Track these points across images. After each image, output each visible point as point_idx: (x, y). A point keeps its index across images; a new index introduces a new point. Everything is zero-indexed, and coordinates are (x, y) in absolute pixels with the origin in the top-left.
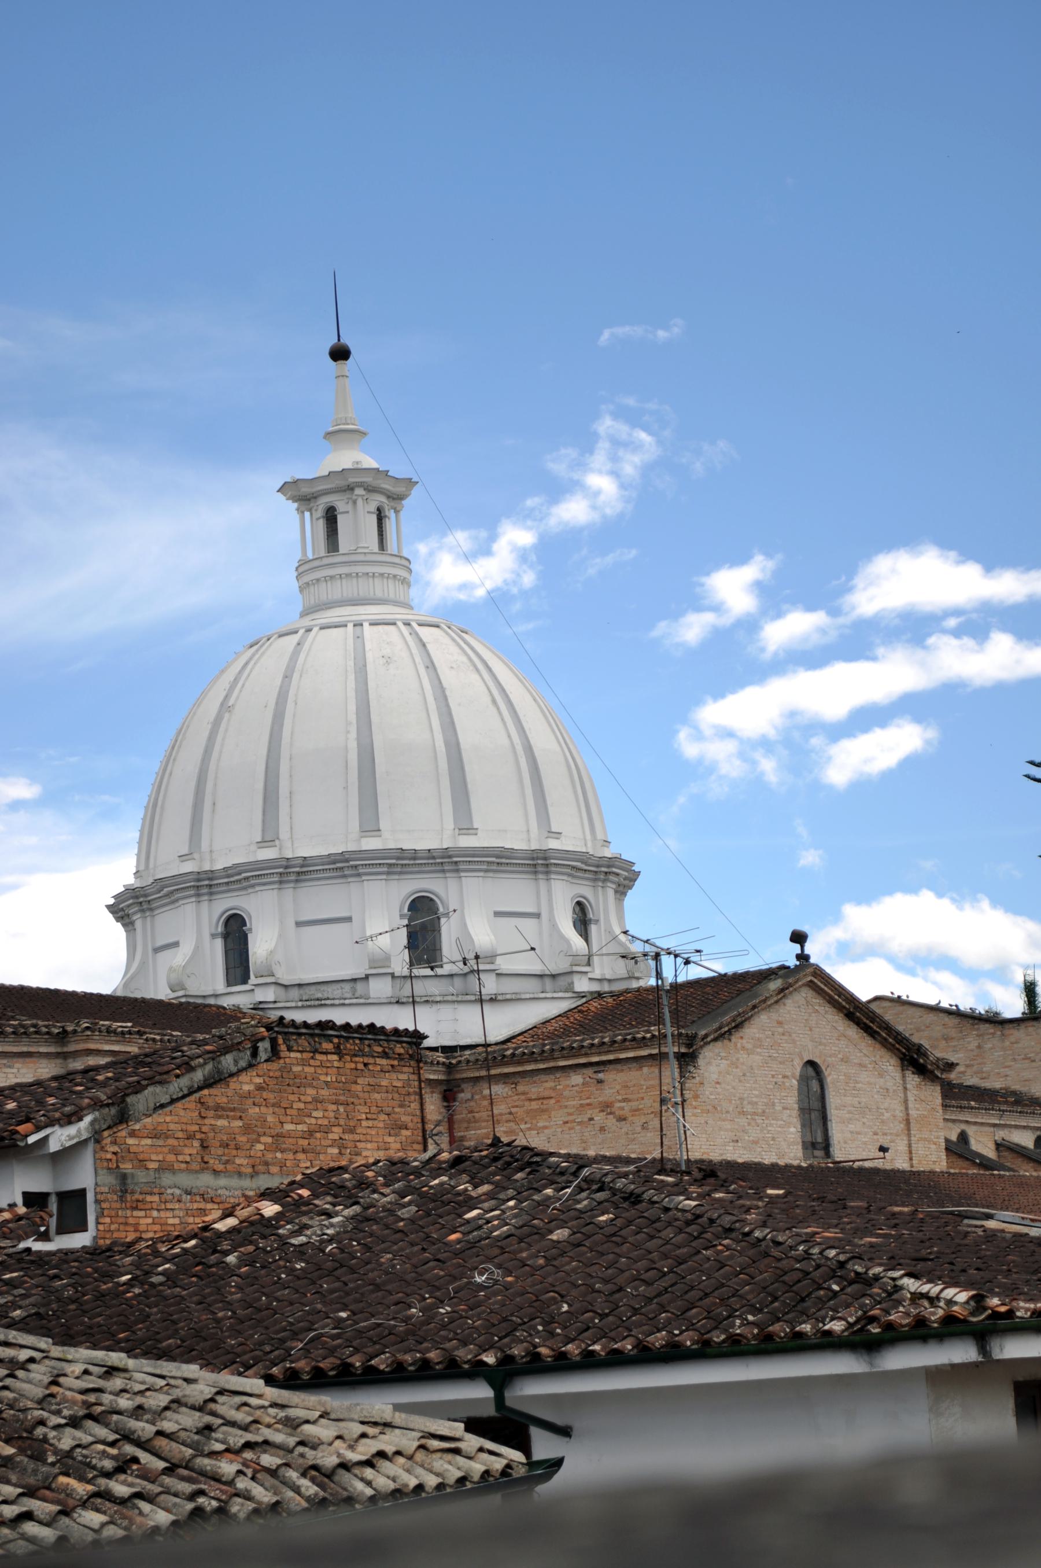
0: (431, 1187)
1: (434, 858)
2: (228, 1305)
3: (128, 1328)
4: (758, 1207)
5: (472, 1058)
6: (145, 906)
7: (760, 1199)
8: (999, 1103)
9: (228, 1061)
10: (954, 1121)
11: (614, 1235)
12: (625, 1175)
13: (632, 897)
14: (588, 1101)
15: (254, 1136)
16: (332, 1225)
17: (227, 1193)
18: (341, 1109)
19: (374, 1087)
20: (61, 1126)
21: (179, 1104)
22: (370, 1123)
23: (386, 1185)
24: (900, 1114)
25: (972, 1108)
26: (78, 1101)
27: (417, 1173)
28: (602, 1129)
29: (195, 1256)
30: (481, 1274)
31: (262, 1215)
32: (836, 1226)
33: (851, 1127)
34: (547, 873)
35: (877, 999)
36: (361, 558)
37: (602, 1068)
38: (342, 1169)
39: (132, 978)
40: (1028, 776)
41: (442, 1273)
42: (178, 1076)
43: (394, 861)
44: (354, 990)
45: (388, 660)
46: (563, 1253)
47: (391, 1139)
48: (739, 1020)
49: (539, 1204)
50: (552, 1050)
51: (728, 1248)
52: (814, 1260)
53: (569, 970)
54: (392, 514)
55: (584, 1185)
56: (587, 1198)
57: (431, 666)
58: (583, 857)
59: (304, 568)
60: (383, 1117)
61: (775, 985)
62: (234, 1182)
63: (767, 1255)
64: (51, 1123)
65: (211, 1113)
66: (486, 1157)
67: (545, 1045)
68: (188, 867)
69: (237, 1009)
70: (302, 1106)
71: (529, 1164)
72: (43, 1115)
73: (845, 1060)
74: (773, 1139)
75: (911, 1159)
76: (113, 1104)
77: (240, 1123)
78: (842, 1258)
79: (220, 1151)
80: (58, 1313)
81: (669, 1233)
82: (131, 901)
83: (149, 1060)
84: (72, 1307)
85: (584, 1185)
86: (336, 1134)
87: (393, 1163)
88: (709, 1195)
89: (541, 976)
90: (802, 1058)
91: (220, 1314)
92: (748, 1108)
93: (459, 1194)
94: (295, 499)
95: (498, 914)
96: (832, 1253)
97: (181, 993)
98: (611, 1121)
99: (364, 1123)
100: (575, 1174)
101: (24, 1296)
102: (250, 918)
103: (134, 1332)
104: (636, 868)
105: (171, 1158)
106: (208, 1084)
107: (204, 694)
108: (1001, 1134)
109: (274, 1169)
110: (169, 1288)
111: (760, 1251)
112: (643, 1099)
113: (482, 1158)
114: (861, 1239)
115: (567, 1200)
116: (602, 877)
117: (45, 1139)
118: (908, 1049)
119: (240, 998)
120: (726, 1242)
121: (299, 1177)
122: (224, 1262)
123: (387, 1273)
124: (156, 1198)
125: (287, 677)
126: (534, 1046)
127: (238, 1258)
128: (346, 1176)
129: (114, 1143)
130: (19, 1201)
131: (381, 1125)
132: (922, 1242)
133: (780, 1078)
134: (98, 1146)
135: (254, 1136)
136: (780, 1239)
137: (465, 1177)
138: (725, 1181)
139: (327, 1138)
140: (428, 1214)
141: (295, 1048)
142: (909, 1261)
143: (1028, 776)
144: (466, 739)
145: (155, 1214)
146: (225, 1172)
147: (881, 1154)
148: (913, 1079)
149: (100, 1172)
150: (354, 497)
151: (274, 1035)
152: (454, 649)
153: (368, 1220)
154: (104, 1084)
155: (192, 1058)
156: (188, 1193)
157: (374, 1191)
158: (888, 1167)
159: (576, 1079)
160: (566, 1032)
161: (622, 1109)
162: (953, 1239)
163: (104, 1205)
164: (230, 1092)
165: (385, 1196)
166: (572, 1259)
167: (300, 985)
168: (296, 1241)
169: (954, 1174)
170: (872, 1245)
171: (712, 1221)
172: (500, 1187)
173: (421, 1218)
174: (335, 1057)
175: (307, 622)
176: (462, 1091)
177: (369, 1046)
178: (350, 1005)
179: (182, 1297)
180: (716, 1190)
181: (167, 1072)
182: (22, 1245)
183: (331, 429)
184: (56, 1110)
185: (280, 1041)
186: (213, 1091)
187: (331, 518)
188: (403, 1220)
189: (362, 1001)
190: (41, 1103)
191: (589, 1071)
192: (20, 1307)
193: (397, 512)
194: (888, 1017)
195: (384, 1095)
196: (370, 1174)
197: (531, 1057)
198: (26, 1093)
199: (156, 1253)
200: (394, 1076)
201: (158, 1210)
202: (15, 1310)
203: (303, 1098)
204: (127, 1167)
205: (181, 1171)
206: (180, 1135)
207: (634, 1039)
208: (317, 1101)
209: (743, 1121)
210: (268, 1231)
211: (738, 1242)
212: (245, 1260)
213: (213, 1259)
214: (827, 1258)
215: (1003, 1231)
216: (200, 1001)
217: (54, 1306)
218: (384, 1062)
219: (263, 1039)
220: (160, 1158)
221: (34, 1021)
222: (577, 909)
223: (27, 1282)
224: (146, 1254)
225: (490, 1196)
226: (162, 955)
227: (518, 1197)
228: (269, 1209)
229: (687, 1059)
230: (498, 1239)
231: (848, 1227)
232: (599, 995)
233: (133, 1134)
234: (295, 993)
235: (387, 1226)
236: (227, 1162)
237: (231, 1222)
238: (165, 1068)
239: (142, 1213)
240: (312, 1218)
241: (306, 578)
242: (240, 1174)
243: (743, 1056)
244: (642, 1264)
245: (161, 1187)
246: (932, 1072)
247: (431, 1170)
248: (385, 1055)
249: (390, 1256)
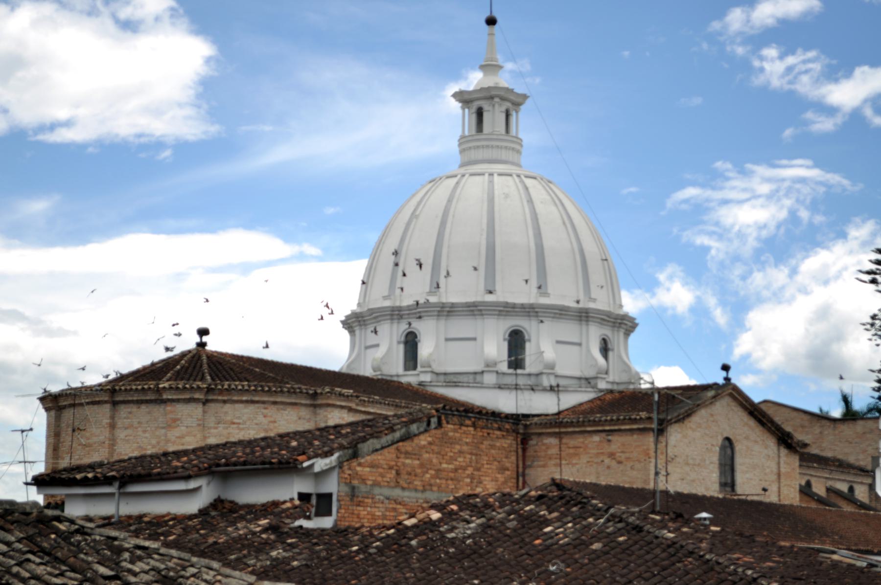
0: (525, 511)
1: (524, 308)
2: (412, 570)
3: (357, 578)
4: (706, 539)
5: (539, 422)
6: (362, 323)
7: (707, 533)
8: (830, 465)
9: (414, 428)
10: (804, 474)
11: (627, 549)
12: (633, 514)
13: (633, 337)
14: (601, 451)
15: (425, 470)
16: (469, 528)
17: (408, 500)
18: (474, 457)
19: (492, 447)
20: (322, 458)
21: (386, 450)
22: (488, 466)
23: (501, 507)
24: (775, 470)
25: (815, 467)
26: (331, 445)
27: (517, 501)
28: (609, 467)
29: (393, 539)
30: (553, 565)
31: (431, 519)
32: (750, 554)
33: (747, 476)
34: (587, 321)
35: (765, 402)
36: (495, 137)
37: (611, 433)
38: (476, 496)
39: (352, 362)
40: (857, 279)
41: (531, 562)
42: (386, 434)
43: (502, 309)
44: (475, 379)
45: (507, 196)
46: (598, 557)
47: (499, 476)
48: (689, 412)
49: (585, 527)
50: (584, 421)
51: (691, 563)
52: (739, 575)
53: (595, 376)
54: (514, 114)
55: (611, 519)
56: (612, 526)
57: (530, 201)
58: (608, 314)
59: (463, 140)
60: (496, 463)
61: (711, 393)
62: (413, 494)
63: (712, 569)
64: (316, 456)
65: (403, 456)
66: (556, 496)
67: (579, 418)
68: (387, 303)
69: (409, 384)
70: (452, 454)
71: (580, 503)
72: (313, 452)
73: (747, 438)
74: (703, 479)
75: (779, 496)
76: (350, 448)
77: (417, 462)
78: (755, 576)
79: (406, 477)
80: (318, 565)
81: (658, 551)
82: (354, 320)
83: (370, 423)
84: (326, 562)
85: (611, 519)
86: (469, 471)
87: (504, 495)
88: (679, 529)
89: (580, 379)
90: (722, 434)
91: (408, 575)
92: (691, 462)
93: (540, 517)
94: (460, 101)
95: (558, 342)
96: (749, 572)
97: (378, 373)
98: (614, 464)
99: (486, 466)
100: (607, 511)
101: (299, 554)
102: (418, 330)
103: (360, 581)
104: (637, 321)
105: (379, 479)
106: (402, 439)
107: (402, 207)
108: (830, 483)
109: (435, 488)
110: (379, 556)
111: (709, 567)
112: (632, 452)
113: (554, 497)
114: (764, 563)
115: (601, 526)
116: (617, 325)
117: (312, 466)
118: (782, 434)
119: (410, 378)
120: (690, 559)
121: (451, 498)
122: (410, 544)
123: (500, 559)
124: (370, 501)
125: (450, 201)
126: (573, 418)
127: (418, 543)
128: (478, 500)
129: (350, 469)
130: (296, 496)
131: (494, 467)
132: (798, 567)
133: (709, 446)
134: (341, 470)
135: (425, 470)
136: (721, 561)
137: (544, 507)
138: (688, 520)
139: (464, 473)
140: (523, 527)
141: (451, 422)
142: (791, 580)
143: (857, 279)
144: (547, 243)
145: (369, 509)
146: (408, 489)
147: (763, 492)
148: (784, 451)
149: (341, 484)
150: (494, 103)
151: (439, 414)
152: (543, 192)
153: (490, 527)
154: (346, 436)
155: (394, 425)
156: (388, 499)
157: (494, 510)
158: (767, 500)
159: (596, 438)
160: (592, 411)
161: (620, 457)
162: (814, 566)
163: (342, 503)
164: (414, 445)
165: (499, 513)
166: (604, 562)
167: (445, 374)
168: (451, 535)
169: (804, 508)
170: (771, 568)
171: (682, 547)
172: (563, 515)
173: (520, 529)
174: (472, 429)
175: (462, 171)
176: (532, 440)
177: (491, 424)
178: (473, 387)
179: (387, 564)
180: (682, 526)
181: (381, 432)
182: (297, 523)
183: (484, 63)
184: (319, 449)
185: (443, 418)
186: (405, 444)
187: (480, 113)
188: (509, 529)
189: (479, 385)
190: (311, 444)
191: (603, 435)
192: (297, 560)
193: (517, 112)
194: (777, 419)
195: (497, 451)
196: (491, 500)
197: (572, 424)
198: (302, 437)
199: (371, 535)
200: (503, 441)
201: (371, 507)
202: (294, 561)
203: (453, 450)
204: (355, 482)
205: (385, 486)
206: (385, 466)
207: (630, 419)
208: (461, 452)
209: (687, 469)
210: (433, 528)
211: (696, 560)
212: (421, 544)
213: (404, 541)
214: (747, 575)
215: (841, 562)
216: (389, 378)
217: (316, 561)
218: (498, 433)
219: (433, 416)
220: (374, 478)
221: (299, 386)
222: (603, 342)
223: (300, 545)
224: (366, 535)
225: (558, 519)
226: (369, 351)
227: (573, 521)
228: (435, 515)
229: (661, 432)
230: (563, 545)
231: (757, 555)
232: (611, 392)
233: (360, 465)
234: (442, 378)
235: (500, 532)
236: (410, 483)
237: (413, 521)
238: (380, 429)
239: (361, 508)
240: (458, 523)
241: (465, 146)
242: (416, 490)
243: (690, 432)
244: (643, 568)
245: (373, 495)
246: (795, 448)
247: (525, 501)
248: (499, 429)
249: (501, 549)
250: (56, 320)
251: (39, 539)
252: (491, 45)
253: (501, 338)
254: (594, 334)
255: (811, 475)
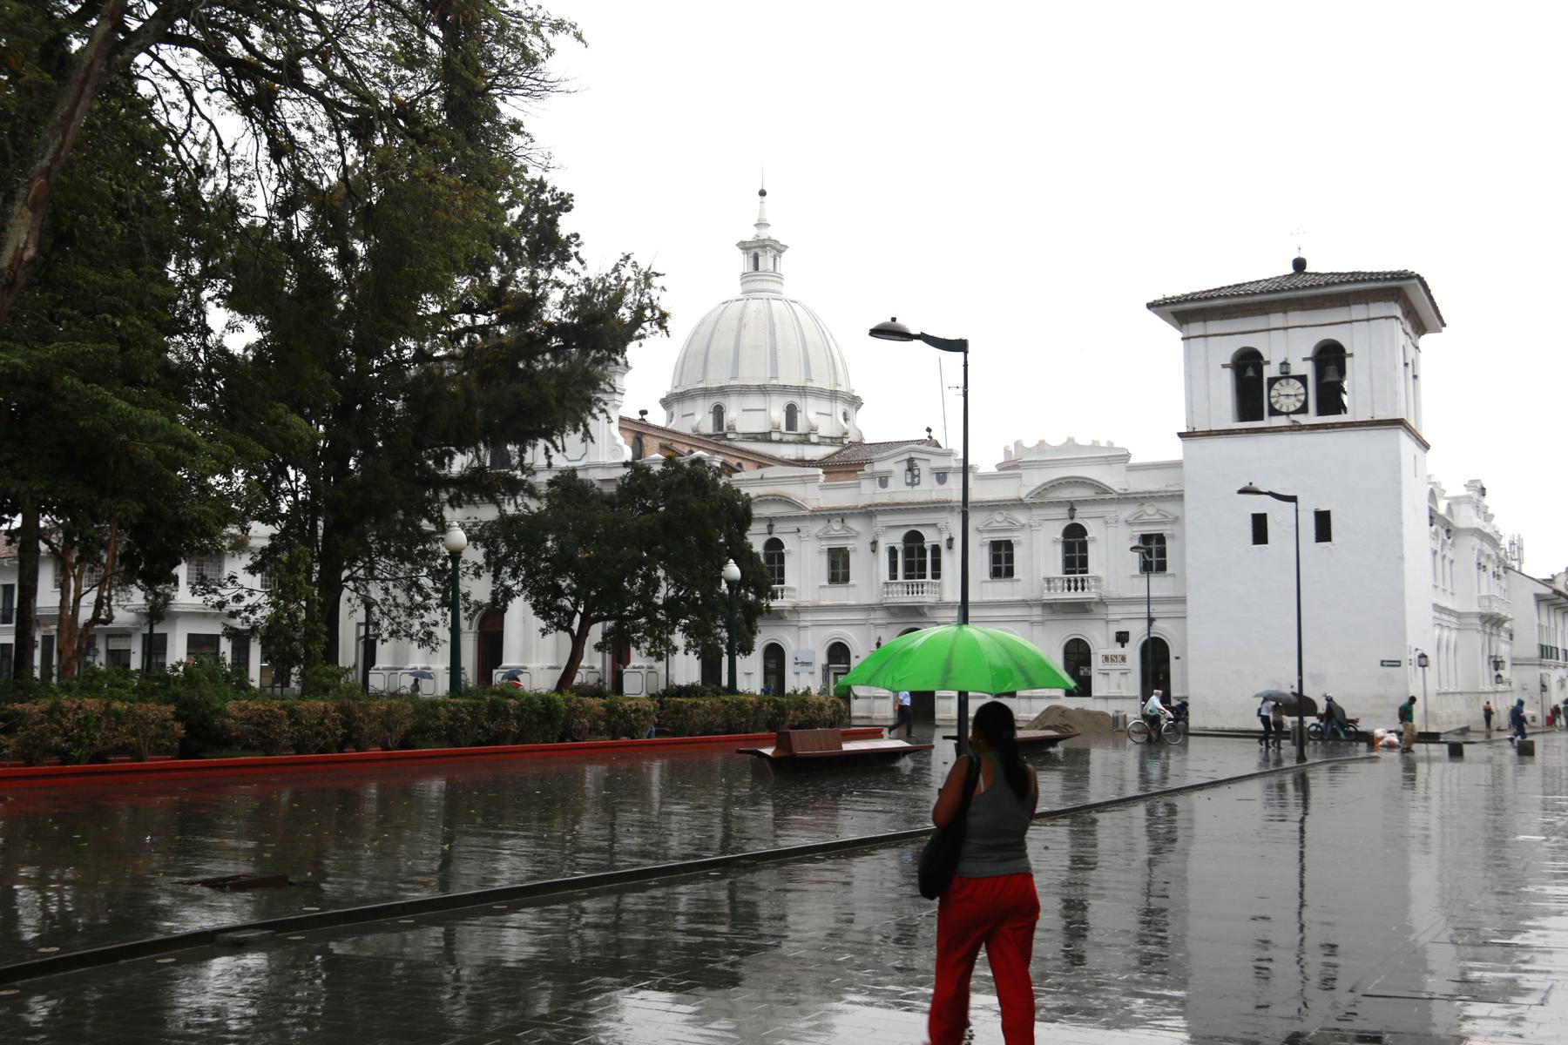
68: (700, 386)
95: (818, 413)
187: (756, 258)
250: (984, 635)
251: (430, 722)
252: (762, 211)
253: (707, 411)
254: (840, 407)
255: (744, 459)
